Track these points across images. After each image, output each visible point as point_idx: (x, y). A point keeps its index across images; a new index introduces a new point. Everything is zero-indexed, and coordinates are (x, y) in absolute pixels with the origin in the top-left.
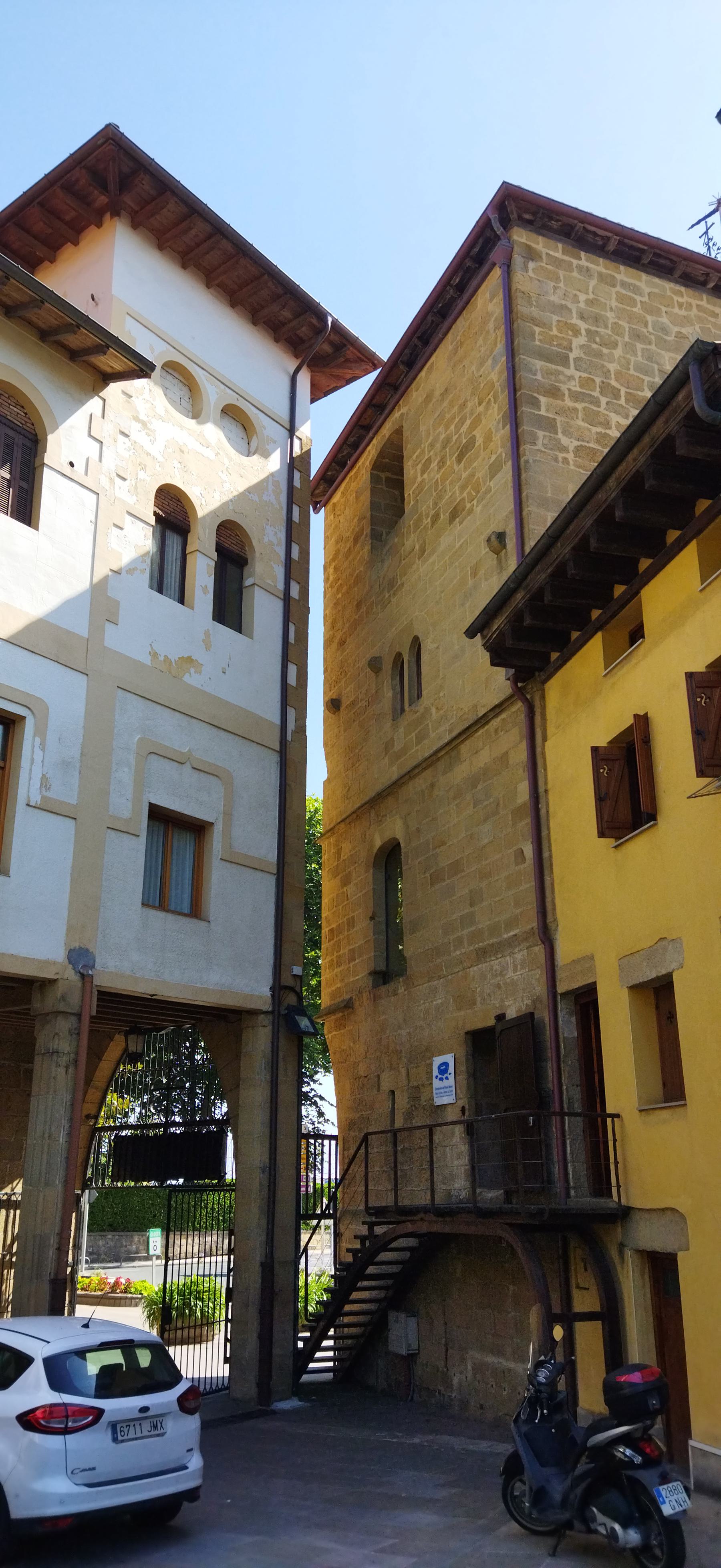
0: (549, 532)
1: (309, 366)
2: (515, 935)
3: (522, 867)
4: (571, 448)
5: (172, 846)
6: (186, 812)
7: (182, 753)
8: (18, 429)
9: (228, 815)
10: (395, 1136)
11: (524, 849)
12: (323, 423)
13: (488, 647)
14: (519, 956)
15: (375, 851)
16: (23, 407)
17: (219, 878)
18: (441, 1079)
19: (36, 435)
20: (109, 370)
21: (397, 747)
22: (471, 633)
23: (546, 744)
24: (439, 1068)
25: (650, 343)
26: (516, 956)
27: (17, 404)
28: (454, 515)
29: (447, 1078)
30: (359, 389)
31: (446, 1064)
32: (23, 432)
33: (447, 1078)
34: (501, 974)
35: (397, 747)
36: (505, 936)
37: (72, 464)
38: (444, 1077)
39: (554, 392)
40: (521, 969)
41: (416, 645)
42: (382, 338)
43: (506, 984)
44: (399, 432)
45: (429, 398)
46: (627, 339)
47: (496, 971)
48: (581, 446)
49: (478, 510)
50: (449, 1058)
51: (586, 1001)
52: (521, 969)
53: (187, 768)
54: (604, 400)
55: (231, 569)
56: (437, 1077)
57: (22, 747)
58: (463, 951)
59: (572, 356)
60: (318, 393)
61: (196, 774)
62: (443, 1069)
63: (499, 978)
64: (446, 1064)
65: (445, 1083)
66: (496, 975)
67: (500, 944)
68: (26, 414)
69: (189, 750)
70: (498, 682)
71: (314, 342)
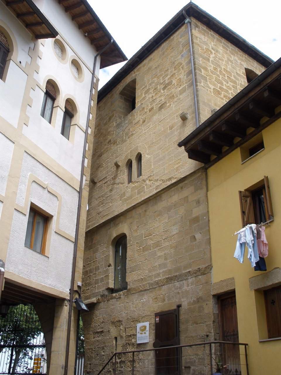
0: (230, 102)
1: (100, 55)
2: (189, 271)
3: (194, 243)
4: (212, 88)
5: (227, 116)
6: (44, 209)
7: (45, 184)
8: (3, 45)
9: (59, 213)
10: (133, 354)
11: (195, 235)
12: (106, 75)
13: (187, 151)
14: (190, 281)
15: (112, 238)
16: (6, 38)
17: (52, 239)
18: (142, 334)
19: (9, 49)
20: (39, 33)
21: (127, 195)
22: (180, 145)
23: (208, 193)
24: (140, 328)
25: (233, 63)
26: (189, 280)
27: (4, 37)
28: (161, 107)
29: (145, 333)
30: (121, 65)
31: (145, 327)
32: (5, 47)
33: (145, 333)
34: (180, 288)
35: (127, 195)
36: (184, 272)
37: (20, 62)
38: (143, 332)
39: (206, 69)
40: (191, 286)
41: (139, 157)
42: (130, 49)
43: (182, 292)
44: (134, 82)
45: (150, 69)
46: (226, 59)
47: (177, 287)
48: (215, 88)
49: (173, 105)
50: (147, 324)
51: (226, 300)
52: (191, 286)
53: (46, 191)
54: (221, 76)
55: (68, 118)
56: (139, 333)
57: (137, 52)
58: (160, 279)
59: (211, 59)
60: (103, 66)
61: (49, 195)
62: (143, 329)
63: (179, 290)
64: (145, 327)
65: (144, 335)
66: (177, 289)
67: (180, 275)
68: (7, 41)
69: (47, 183)
70: (188, 165)
71: (105, 48)
